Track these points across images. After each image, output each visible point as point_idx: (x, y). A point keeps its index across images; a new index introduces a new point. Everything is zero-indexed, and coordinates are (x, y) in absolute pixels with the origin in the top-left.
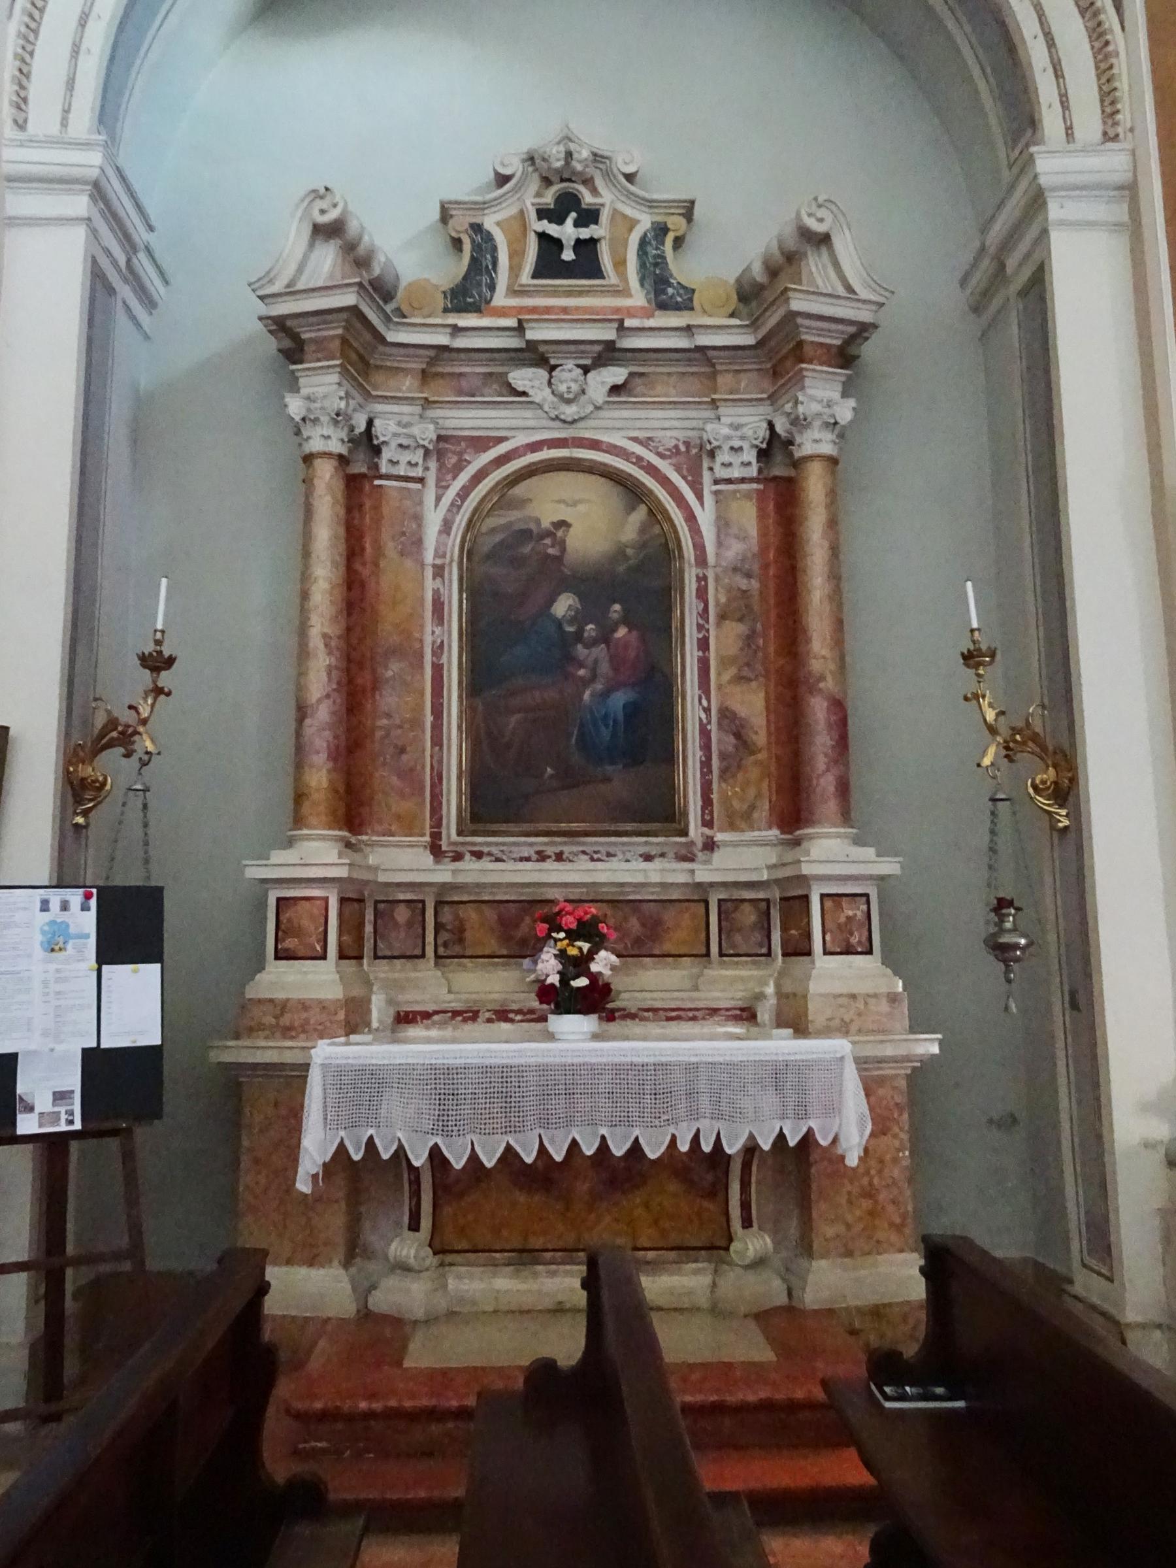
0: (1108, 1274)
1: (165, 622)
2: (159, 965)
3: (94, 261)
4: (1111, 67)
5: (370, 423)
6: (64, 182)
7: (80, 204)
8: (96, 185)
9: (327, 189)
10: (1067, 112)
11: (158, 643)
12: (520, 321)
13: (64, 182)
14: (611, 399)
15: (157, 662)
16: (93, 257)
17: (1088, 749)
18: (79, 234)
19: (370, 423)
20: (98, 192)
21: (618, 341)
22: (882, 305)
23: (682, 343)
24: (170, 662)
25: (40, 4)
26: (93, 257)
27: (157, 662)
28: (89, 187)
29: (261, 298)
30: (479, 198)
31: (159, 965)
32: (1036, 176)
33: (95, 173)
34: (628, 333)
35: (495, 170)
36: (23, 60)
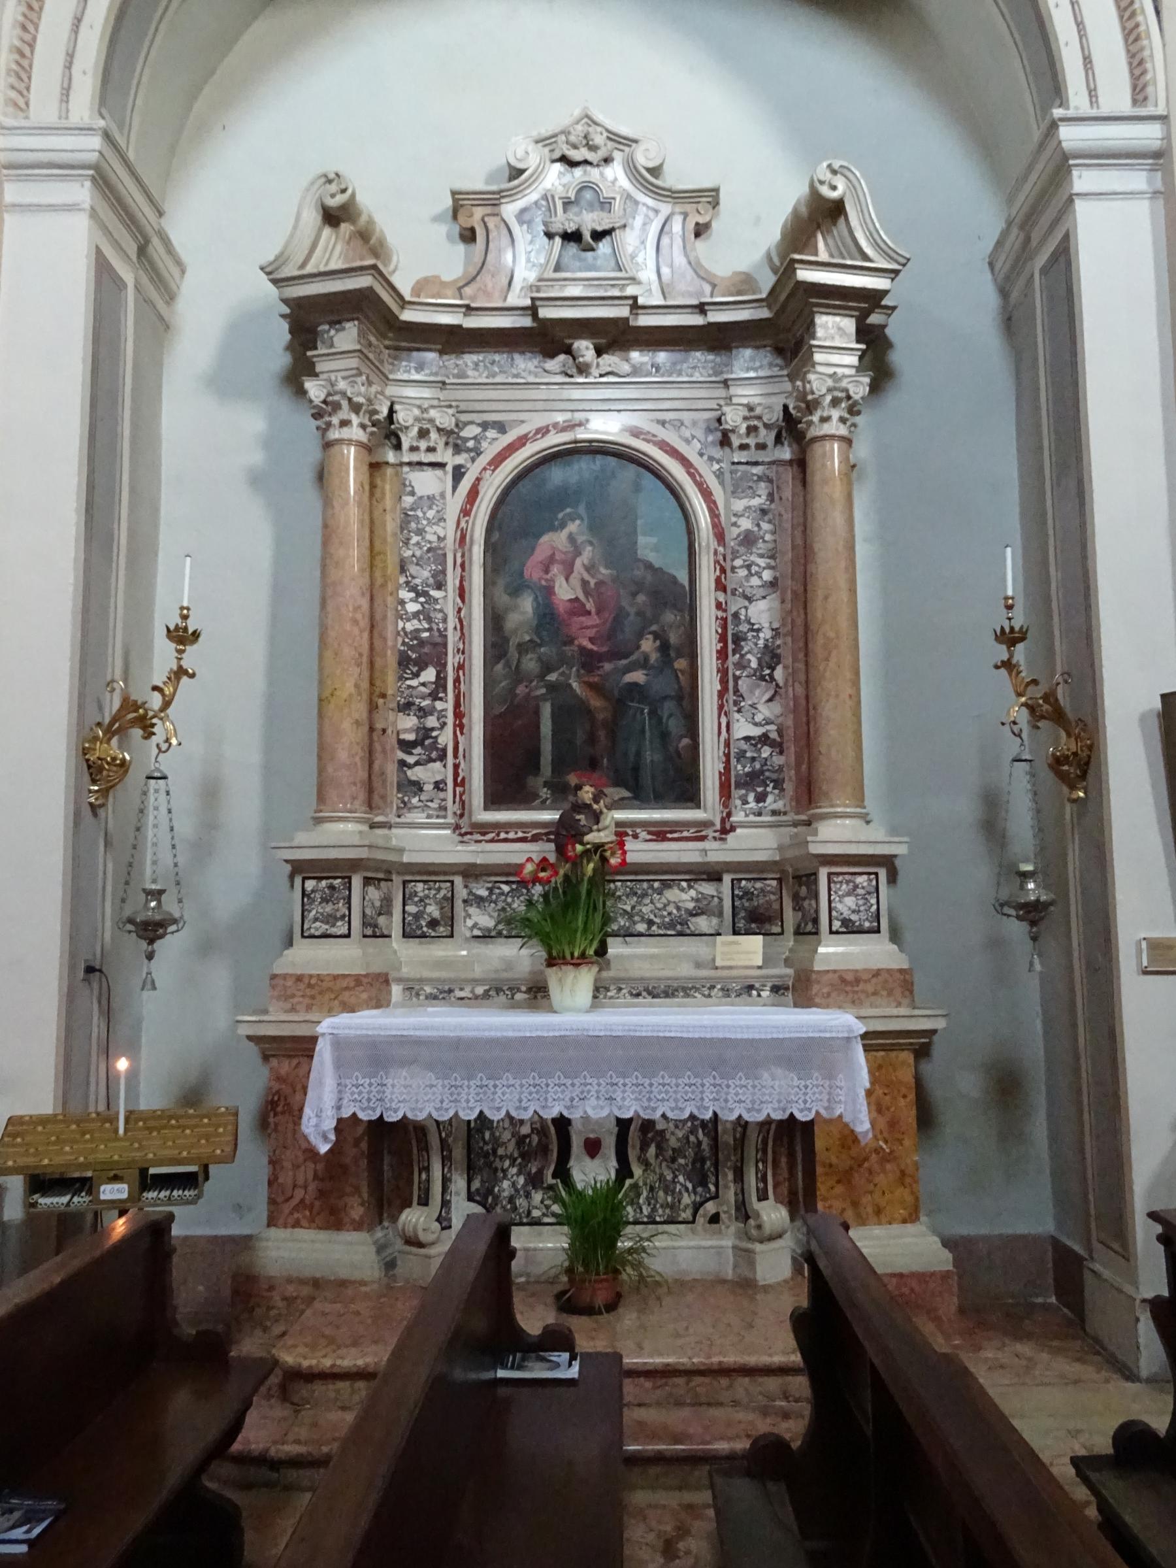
0: (1120, 1250)
1: (189, 601)
2: (513, 1228)
3: (99, 251)
4: (1137, 25)
5: (391, 411)
6: (63, 168)
7: (82, 192)
8: (96, 167)
9: (337, 175)
10: (1090, 72)
11: (185, 618)
12: (533, 299)
13: (63, 168)
14: (557, 199)
15: (183, 637)
16: (97, 247)
17: (1115, 855)
18: (81, 224)
19: (391, 411)
20: (102, 182)
21: (631, 318)
22: (896, 272)
23: (697, 320)
24: (196, 635)
25: (36, 6)
26: (97, 247)
27: (183, 637)
28: (91, 172)
29: (275, 282)
30: (494, 188)
31: (513, 1228)
32: (1060, 142)
33: (93, 157)
34: (640, 311)
35: (509, 164)
36: (22, 55)
